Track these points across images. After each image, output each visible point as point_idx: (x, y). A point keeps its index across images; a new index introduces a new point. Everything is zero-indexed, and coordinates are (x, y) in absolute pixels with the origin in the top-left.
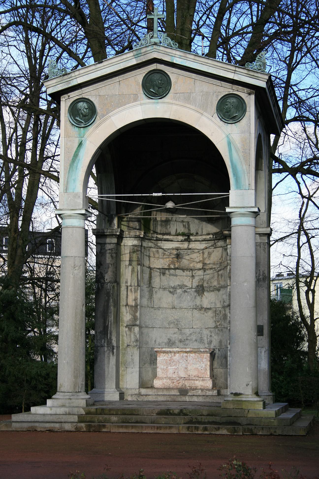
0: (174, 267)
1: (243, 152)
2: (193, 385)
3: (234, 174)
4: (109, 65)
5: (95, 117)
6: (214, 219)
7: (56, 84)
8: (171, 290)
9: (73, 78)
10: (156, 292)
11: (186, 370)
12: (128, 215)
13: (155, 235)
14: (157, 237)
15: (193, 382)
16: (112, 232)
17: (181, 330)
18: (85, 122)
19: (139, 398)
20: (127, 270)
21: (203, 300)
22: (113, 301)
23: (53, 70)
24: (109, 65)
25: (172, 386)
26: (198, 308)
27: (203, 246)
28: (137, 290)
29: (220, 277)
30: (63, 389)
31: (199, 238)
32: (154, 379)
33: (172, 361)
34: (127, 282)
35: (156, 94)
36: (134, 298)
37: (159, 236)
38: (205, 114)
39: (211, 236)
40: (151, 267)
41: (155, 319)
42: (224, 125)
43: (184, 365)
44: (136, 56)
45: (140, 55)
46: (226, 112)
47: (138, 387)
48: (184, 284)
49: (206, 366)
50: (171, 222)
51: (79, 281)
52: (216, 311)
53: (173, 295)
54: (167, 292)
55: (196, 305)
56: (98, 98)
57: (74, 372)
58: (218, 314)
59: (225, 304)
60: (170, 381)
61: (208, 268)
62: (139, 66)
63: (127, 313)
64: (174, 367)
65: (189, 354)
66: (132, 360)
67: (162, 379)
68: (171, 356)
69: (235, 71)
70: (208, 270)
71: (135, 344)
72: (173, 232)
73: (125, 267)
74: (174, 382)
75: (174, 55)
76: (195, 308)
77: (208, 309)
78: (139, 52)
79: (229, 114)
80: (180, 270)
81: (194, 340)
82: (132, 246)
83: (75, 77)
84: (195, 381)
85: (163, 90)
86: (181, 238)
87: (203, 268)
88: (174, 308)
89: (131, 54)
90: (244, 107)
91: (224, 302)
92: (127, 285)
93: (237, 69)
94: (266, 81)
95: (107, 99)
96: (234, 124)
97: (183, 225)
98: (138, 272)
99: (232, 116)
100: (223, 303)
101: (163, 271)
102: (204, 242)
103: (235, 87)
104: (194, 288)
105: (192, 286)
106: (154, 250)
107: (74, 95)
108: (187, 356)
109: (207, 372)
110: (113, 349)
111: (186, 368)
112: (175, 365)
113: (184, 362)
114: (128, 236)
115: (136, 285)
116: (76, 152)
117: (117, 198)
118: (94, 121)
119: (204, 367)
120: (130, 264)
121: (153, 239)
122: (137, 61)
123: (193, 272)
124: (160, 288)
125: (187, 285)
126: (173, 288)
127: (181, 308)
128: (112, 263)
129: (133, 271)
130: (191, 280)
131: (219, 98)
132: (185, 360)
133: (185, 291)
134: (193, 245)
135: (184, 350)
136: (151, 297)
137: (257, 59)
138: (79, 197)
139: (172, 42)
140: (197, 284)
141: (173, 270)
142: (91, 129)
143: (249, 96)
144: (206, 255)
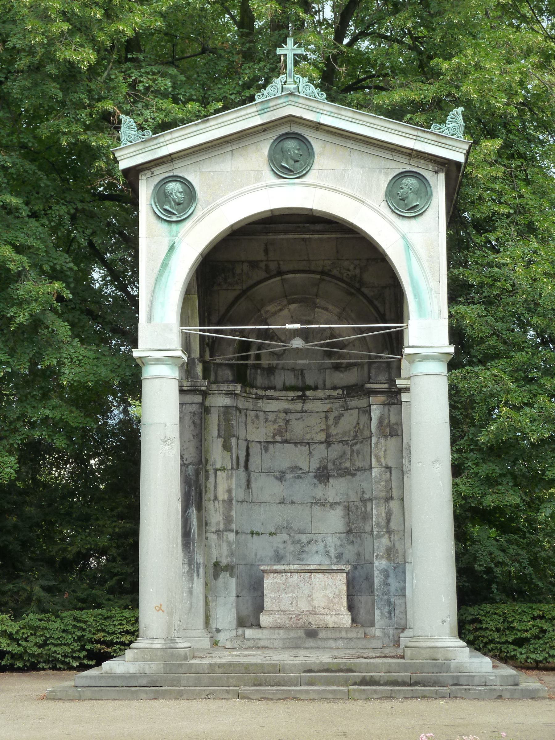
2: (322, 623)
3: (415, 295)
5: (194, 205)
6: (344, 366)
9: (161, 145)
12: (215, 360)
13: (254, 391)
14: (256, 394)
15: (321, 617)
23: (128, 132)
27: (324, 407)
29: (355, 454)
30: (150, 634)
31: (320, 393)
35: (290, 171)
36: (226, 488)
43: (307, 592)
44: (261, 112)
45: (268, 110)
47: (234, 627)
50: (277, 371)
53: (280, 483)
56: (198, 177)
59: (365, 496)
63: (216, 511)
64: (290, 595)
67: (271, 613)
68: (285, 577)
75: (320, 111)
77: (336, 503)
83: (164, 144)
84: (325, 616)
85: (301, 164)
86: (292, 394)
87: (326, 441)
89: (254, 109)
93: (420, 134)
94: (465, 152)
99: (411, 206)
101: (266, 445)
102: (328, 401)
106: (252, 413)
107: (161, 173)
108: (310, 578)
109: (342, 603)
110: (198, 567)
111: (310, 596)
112: (293, 592)
116: (164, 260)
117: (201, 330)
118: (193, 212)
121: (251, 396)
125: (301, 466)
128: (195, 434)
132: (307, 584)
133: (299, 477)
134: (309, 406)
135: (307, 568)
138: (171, 330)
140: (318, 466)
142: (187, 224)
144: (331, 421)
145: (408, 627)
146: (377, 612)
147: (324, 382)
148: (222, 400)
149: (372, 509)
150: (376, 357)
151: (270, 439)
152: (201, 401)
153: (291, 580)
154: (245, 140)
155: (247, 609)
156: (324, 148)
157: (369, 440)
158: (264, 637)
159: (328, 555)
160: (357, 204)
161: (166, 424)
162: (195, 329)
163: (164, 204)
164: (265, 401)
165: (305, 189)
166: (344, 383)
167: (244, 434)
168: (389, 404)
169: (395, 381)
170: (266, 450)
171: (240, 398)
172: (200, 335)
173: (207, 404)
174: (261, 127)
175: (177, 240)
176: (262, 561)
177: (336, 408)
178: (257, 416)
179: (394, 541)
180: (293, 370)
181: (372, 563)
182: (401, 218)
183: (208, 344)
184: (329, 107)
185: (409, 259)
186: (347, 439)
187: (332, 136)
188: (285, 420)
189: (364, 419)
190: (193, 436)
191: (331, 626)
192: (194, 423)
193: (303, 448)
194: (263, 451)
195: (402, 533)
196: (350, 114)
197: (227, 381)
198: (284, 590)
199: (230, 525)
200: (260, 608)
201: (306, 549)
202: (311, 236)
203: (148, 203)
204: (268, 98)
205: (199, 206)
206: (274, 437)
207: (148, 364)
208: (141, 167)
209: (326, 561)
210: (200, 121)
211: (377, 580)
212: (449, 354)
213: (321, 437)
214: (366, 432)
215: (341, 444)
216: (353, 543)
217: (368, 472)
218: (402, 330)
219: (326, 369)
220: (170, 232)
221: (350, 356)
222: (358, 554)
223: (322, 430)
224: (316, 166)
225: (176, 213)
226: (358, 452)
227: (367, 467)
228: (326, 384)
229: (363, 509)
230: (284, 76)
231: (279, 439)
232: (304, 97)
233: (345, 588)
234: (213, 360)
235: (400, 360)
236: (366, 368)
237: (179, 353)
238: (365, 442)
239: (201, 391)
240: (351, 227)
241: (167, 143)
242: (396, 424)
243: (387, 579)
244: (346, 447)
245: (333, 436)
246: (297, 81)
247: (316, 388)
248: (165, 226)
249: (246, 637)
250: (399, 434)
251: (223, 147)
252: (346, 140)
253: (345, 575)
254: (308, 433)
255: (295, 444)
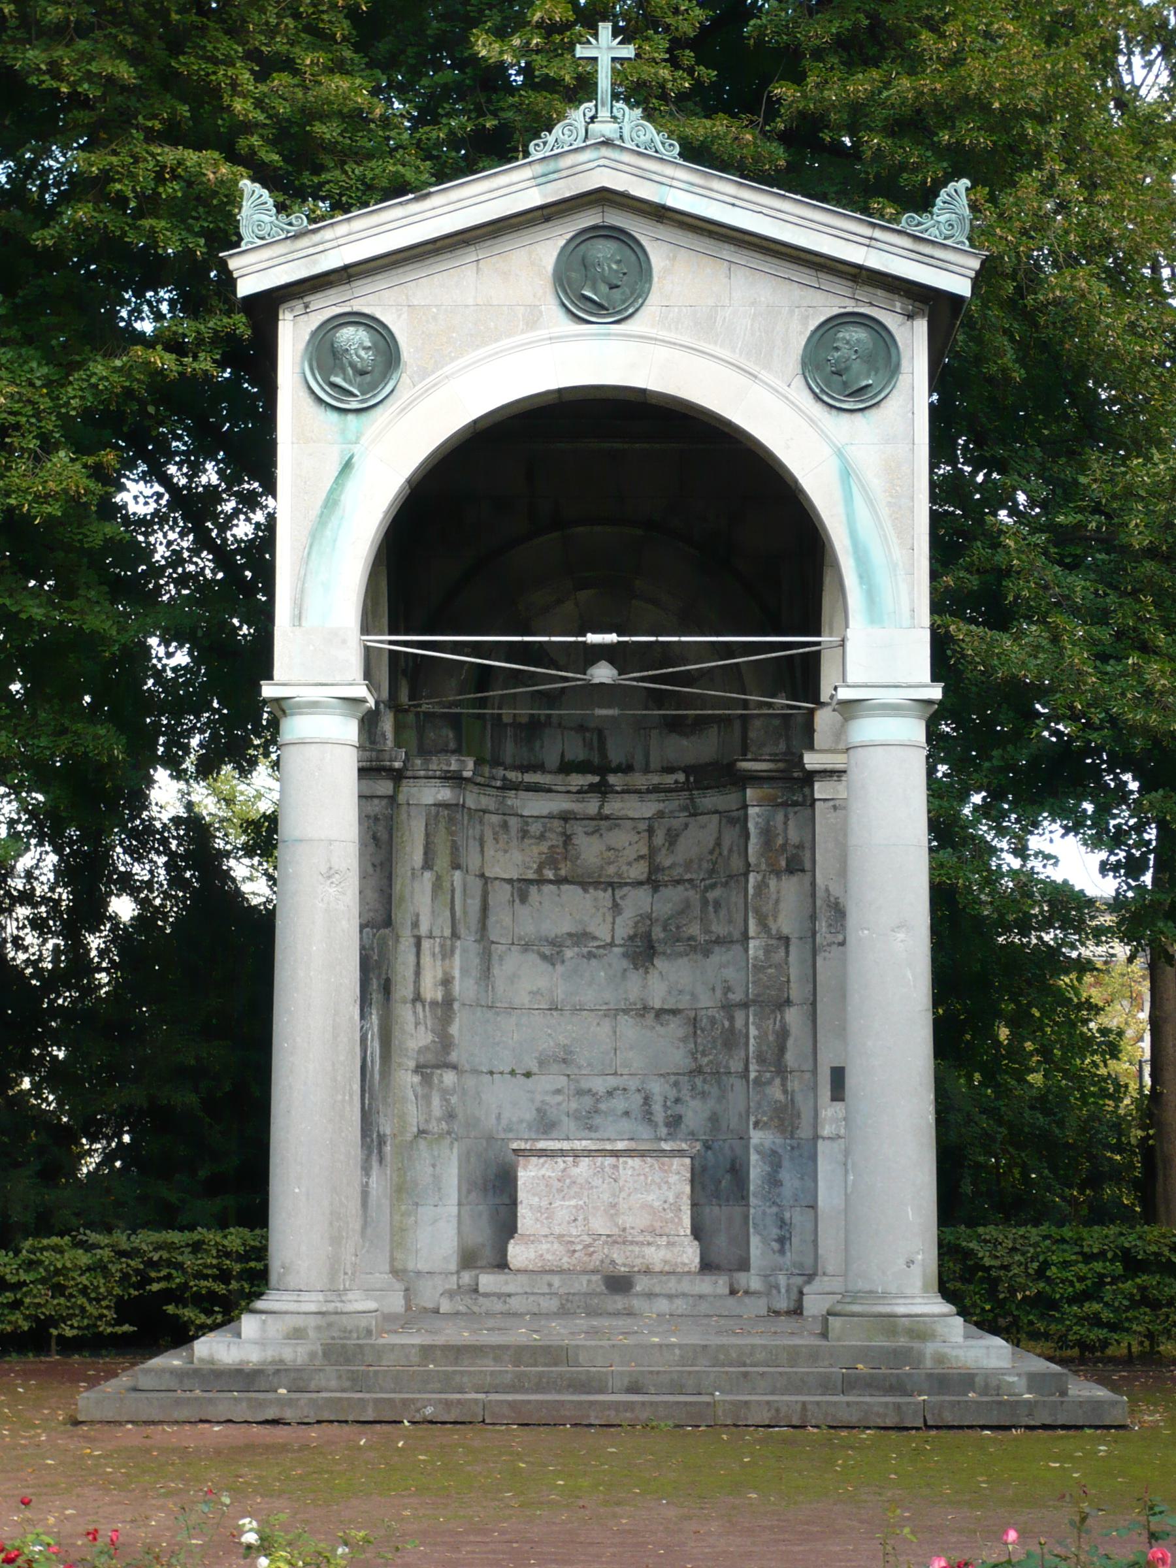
0: (555, 875)
1: (889, 504)
3: (861, 577)
4: (451, 207)
5: (395, 376)
7: (270, 263)
8: (547, 950)
10: (501, 958)
11: (612, 1212)
12: (420, 705)
13: (500, 772)
14: (504, 779)
15: (637, 1249)
16: (378, 760)
17: (578, 1081)
18: (363, 394)
19: (475, 1304)
20: (416, 885)
21: (650, 983)
22: (379, 985)
23: (256, 217)
24: (451, 207)
25: (566, 1262)
26: (632, 1010)
27: (646, 808)
28: (452, 952)
29: (711, 909)
31: (639, 780)
32: (507, 1243)
33: (568, 1181)
34: (416, 925)
35: (601, 306)
36: (440, 975)
37: (513, 775)
38: (764, 375)
39: (681, 777)
40: (487, 874)
41: (498, 1044)
42: (826, 415)
44: (541, 180)
45: (555, 176)
46: (833, 373)
48: (588, 930)
49: (677, 1196)
51: (344, 923)
52: (695, 1019)
53: (551, 968)
54: (532, 957)
55: (626, 999)
56: (405, 316)
57: (331, 1224)
58: (703, 1030)
59: (730, 996)
60: (561, 1248)
61: (666, 878)
62: (545, 212)
63: (417, 1024)
64: (573, 1202)
65: (621, 1160)
66: (437, 1179)
67: (531, 1239)
68: (562, 1165)
69: (871, 238)
70: (666, 886)
71: (444, 1125)
72: (553, 760)
73: (409, 873)
74: (574, 1251)
76: (623, 1010)
78: (552, 165)
79: (844, 378)
80: (572, 887)
81: (619, 1113)
82: (435, 805)
83: (334, 244)
85: (623, 293)
86: (578, 780)
87: (649, 881)
88: (556, 1009)
89: (527, 173)
90: (894, 359)
91: (728, 989)
92: (416, 932)
93: (878, 234)
94: (972, 274)
95: (435, 318)
96: (859, 415)
97: (584, 740)
98: (453, 891)
100: (725, 994)
101: (522, 888)
102: (653, 796)
103: (863, 293)
104: (621, 946)
105: (613, 937)
106: (495, 819)
107: (325, 307)
108: (615, 1167)
109: (680, 1219)
111: (614, 1206)
112: (577, 1195)
113: (605, 1186)
114: (422, 773)
115: (447, 932)
116: (332, 491)
118: (392, 391)
119: (671, 1200)
120: (428, 865)
121: (493, 784)
122: (545, 196)
123: (617, 892)
124: (513, 944)
125: (597, 934)
126: (552, 943)
127: (578, 1009)
128: (377, 862)
129: (437, 886)
130: (609, 919)
131: (812, 328)
133: (590, 956)
134: (614, 806)
135: (609, 1147)
136: (486, 973)
137: (939, 201)
138: (344, 642)
139: (658, 139)
140: (631, 933)
141: (551, 886)
142: (380, 416)
143: (909, 323)
145: (820, 1272)
146: (755, 1241)
147: (647, 756)
148: (434, 790)
149: (747, 1024)
150: (761, 705)
151: (531, 875)
152: (390, 792)
153: (575, 1171)
154: (504, 238)
155: (481, 1235)
156: (675, 258)
157: (742, 879)
158: (520, 1290)
159: (650, 1120)
160: (743, 379)
161: (330, 842)
162: (382, 641)
163: (332, 371)
164: (522, 794)
165: (633, 345)
166: (689, 759)
167: (478, 863)
168: (784, 804)
169: (801, 757)
170: (524, 898)
171: (470, 787)
172: (390, 651)
173: (402, 798)
174: (539, 213)
175: (356, 449)
176: (511, 1130)
177: (671, 812)
178: (505, 826)
179: (793, 1091)
180: (581, 728)
181: (744, 1138)
182: (834, 412)
183: (404, 673)
184: (685, 174)
185: (848, 499)
186: (694, 876)
187: (690, 235)
188: (564, 834)
189: (730, 836)
190: (374, 865)
191: (657, 1269)
192: (375, 838)
193: (601, 894)
194: (517, 901)
195: (808, 1076)
196: (730, 189)
197: (445, 751)
198: (560, 1190)
199: (448, 1054)
200: (506, 1226)
201: (603, 1106)
202: (626, 446)
203: (298, 370)
204: (556, 151)
205: (405, 379)
206: (539, 870)
207: (292, 714)
208: (282, 292)
209: (645, 1131)
210: (411, 196)
211: (756, 1171)
212: (929, 702)
213: (639, 871)
214: (736, 864)
215: (680, 888)
216: (704, 1095)
217: (738, 948)
218: (819, 652)
219: (650, 728)
220: (343, 432)
221: (703, 701)
222: (714, 1119)
223: (642, 857)
224: (654, 298)
225: (356, 392)
226: (717, 904)
227: (737, 935)
228: (652, 759)
229: (727, 1024)
230: (591, 104)
231: (549, 874)
232: (633, 151)
233: (688, 1189)
234: (415, 706)
235: (811, 712)
236: (737, 725)
237: (361, 691)
238: (732, 884)
239: (391, 770)
240: (726, 430)
241: (341, 241)
242: (800, 846)
243: (776, 1172)
244: (691, 893)
245: (663, 869)
246: (619, 115)
247: (627, 769)
248: (334, 417)
249: (481, 1289)
250: (808, 866)
251: (459, 252)
252: (721, 244)
253: (688, 1161)
254: (609, 863)
255: (584, 885)
